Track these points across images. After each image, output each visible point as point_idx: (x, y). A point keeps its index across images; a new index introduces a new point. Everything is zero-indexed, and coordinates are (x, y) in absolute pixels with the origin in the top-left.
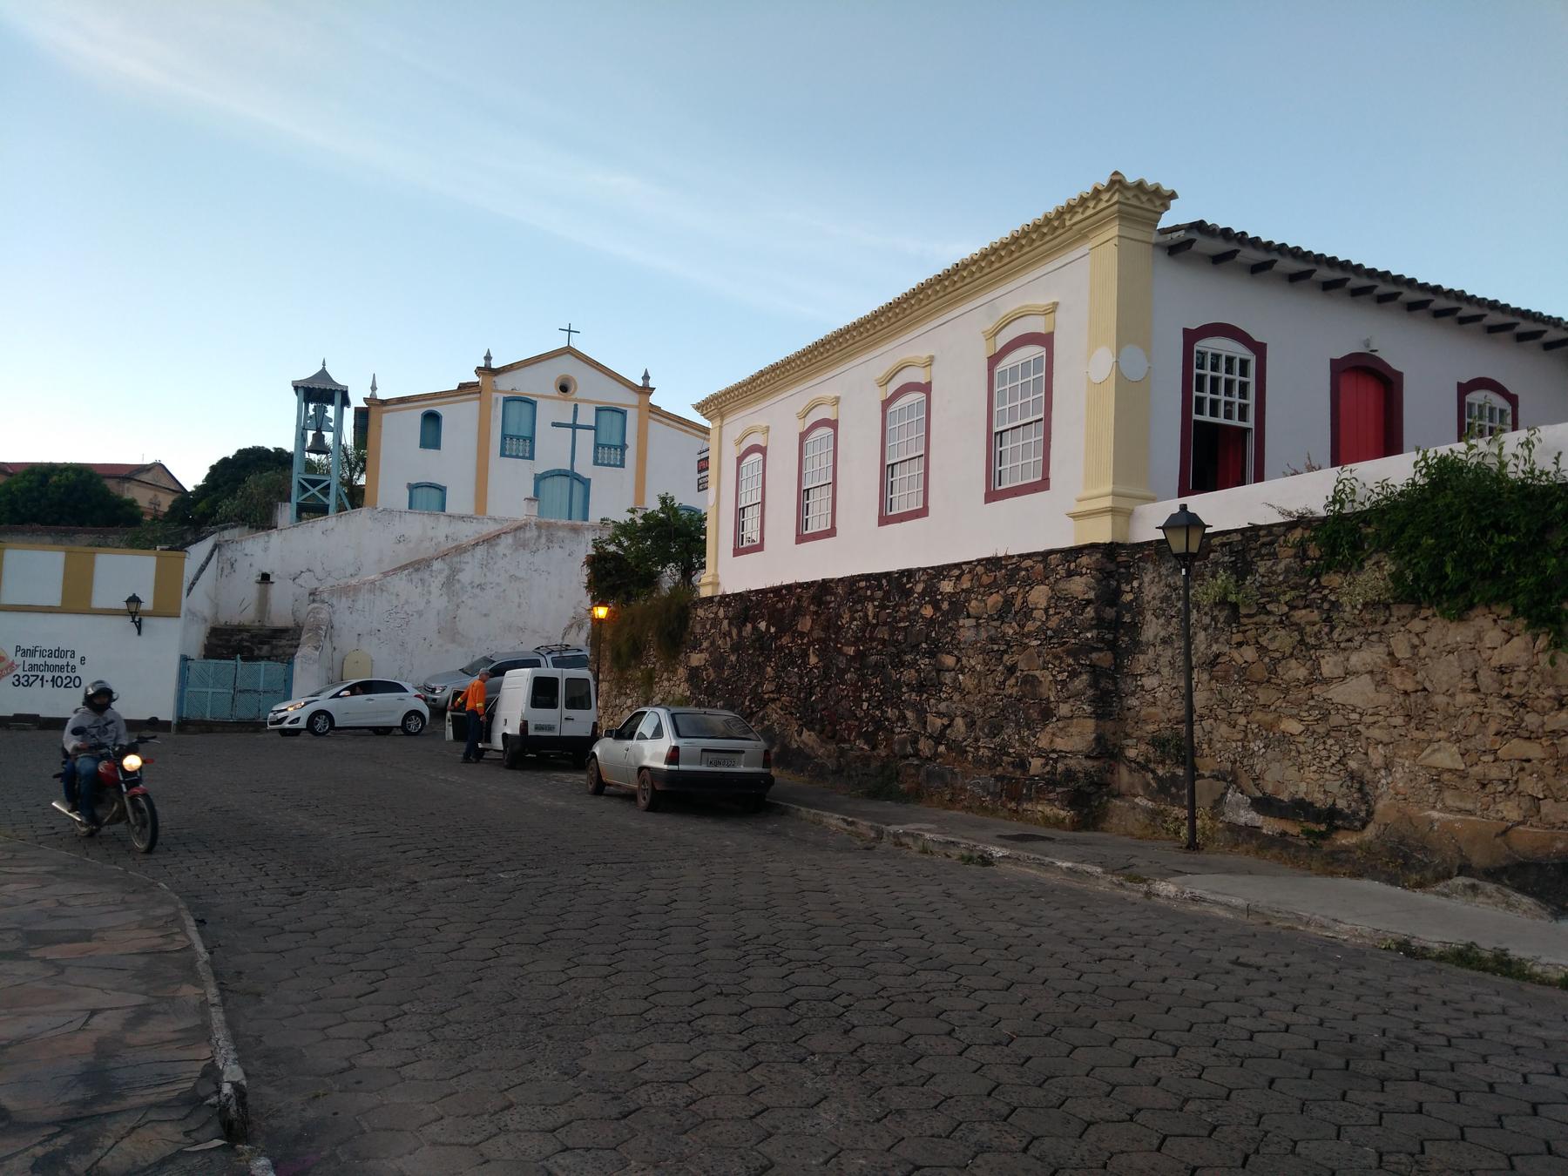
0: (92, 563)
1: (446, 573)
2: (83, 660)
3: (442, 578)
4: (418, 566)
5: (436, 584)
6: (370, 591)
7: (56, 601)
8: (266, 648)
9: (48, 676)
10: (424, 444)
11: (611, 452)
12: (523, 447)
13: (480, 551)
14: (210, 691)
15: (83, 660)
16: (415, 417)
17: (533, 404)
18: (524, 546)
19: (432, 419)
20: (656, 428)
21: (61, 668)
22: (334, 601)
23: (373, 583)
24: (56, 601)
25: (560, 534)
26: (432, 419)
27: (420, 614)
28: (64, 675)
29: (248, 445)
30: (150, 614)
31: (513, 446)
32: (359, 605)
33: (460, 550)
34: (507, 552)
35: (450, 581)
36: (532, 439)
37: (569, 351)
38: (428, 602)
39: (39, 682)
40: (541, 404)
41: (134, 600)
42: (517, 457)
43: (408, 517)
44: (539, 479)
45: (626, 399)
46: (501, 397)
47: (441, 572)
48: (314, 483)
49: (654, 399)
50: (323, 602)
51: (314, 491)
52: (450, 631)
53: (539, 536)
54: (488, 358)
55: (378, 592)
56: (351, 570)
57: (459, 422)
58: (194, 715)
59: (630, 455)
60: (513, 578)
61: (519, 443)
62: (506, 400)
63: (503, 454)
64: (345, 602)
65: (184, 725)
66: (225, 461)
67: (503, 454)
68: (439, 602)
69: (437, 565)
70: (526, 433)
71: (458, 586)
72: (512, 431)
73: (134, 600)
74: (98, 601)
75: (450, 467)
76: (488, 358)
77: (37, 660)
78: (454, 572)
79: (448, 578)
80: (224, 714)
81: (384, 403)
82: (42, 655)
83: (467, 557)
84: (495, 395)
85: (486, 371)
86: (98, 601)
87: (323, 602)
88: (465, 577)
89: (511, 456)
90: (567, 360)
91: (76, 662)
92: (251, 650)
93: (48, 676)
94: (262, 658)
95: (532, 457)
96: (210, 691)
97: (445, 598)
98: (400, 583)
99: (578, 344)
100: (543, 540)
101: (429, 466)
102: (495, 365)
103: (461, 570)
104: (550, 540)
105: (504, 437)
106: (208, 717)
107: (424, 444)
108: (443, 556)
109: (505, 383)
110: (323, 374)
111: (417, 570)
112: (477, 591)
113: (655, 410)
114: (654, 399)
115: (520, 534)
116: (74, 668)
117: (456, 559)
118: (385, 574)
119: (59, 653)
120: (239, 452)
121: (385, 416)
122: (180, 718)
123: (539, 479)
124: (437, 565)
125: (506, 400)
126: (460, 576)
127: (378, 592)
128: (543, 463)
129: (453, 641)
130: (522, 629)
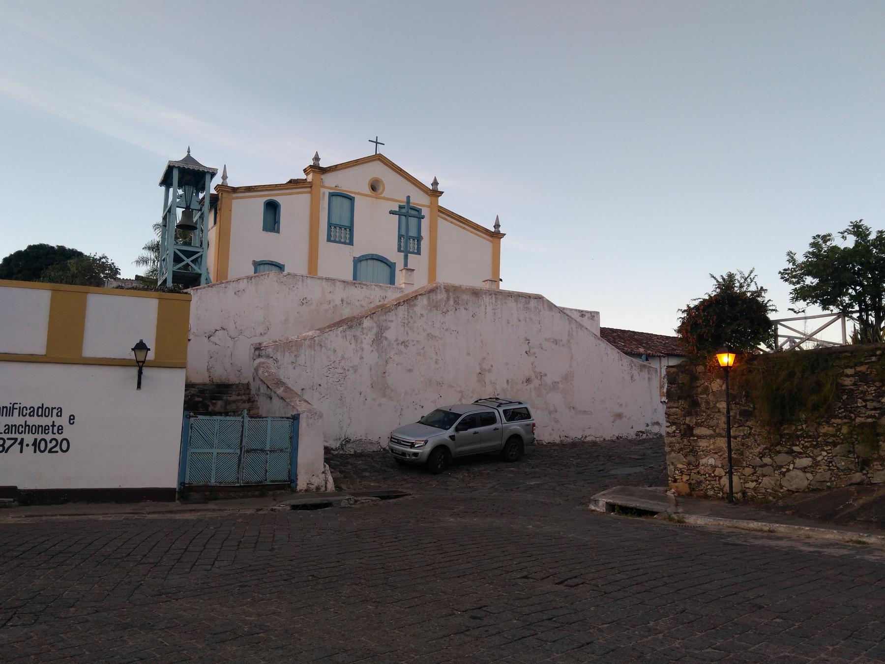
0: (86, 299)
1: (375, 330)
2: (72, 418)
3: (371, 336)
4: (351, 323)
6: (311, 347)
7: (39, 347)
9: (29, 438)
10: (266, 228)
11: (409, 242)
12: (345, 234)
13: (402, 310)
14: (215, 451)
15: (72, 418)
16: (258, 204)
17: (351, 199)
18: (436, 307)
19: (272, 207)
20: (444, 225)
21: (45, 429)
22: (279, 356)
23: (312, 338)
24: (39, 347)
25: (465, 297)
26: (272, 207)
27: (355, 369)
28: (48, 437)
29: (36, 242)
30: (156, 365)
32: (301, 360)
33: (384, 309)
34: (424, 312)
35: (379, 338)
36: (351, 228)
37: (379, 158)
39: (17, 447)
40: (358, 200)
41: (141, 347)
42: (340, 242)
43: (309, 281)
44: (357, 261)
47: (370, 329)
49: (442, 202)
50: (268, 357)
51: (188, 261)
52: (381, 385)
53: (448, 299)
54: (317, 158)
55: (317, 348)
56: (261, 329)
57: (294, 208)
58: (198, 480)
59: (425, 244)
60: (430, 336)
61: (342, 231)
62: (332, 195)
63: (329, 240)
65: (186, 493)
66: (19, 253)
67: (329, 240)
68: (371, 358)
69: (367, 323)
70: (346, 223)
71: (385, 343)
72: (335, 221)
73: (141, 347)
74: (90, 350)
76: (317, 158)
77: (16, 420)
80: (230, 477)
81: (235, 190)
82: (21, 413)
83: (391, 316)
84: (322, 190)
85: (315, 168)
86: (90, 350)
87: (268, 357)
91: (63, 421)
92: (206, 406)
93: (29, 438)
94: (216, 414)
95: (351, 243)
96: (215, 451)
97: (375, 354)
98: (336, 339)
99: (381, 150)
100: (451, 302)
101: (270, 246)
102: (323, 164)
103: (387, 328)
104: (456, 302)
105: (330, 226)
106: (213, 482)
107: (266, 228)
108: (372, 314)
109: (331, 181)
110: (189, 159)
111: (350, 327)
112: (402, 348)
113: (442, 210)
114: (442, 202)
115: (433, 296)
116: (60, 429)
117: (382, 318)
118: (322, 330)
119: (43, 411)
120: (30, 247)
121: (234, 202)
122: (182, 483)
123: (357, 261)
124: (367, 323)
125: (332, 195)
126: (387, 334)
127: (317, 348)
128: (362, 247)
129: (384, 395)
130: (439, 384)
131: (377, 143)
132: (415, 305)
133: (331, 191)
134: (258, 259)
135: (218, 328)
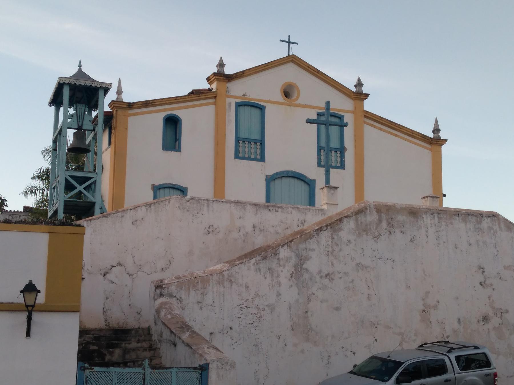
1: (293, 261)
3: (289, 268)
4: (265, 253)
5: (285, 273)
6: (219, 283)
8: (118, 352)
11: (331, 155)
12: (255, 149)
13: (325, 236)
16: (156, 121)
17: (262, 109)
19: (172, 123)
20: (371, 133)
22: (183, 295)
23: (221, 273)
25: (400, 218)
26: (172, 123)
27: (272, 308)
31: (245, 148)
32: (209, 299)
33: (304, 236)
34: (352, 237)
35: (298, 271)
36: (262, 142)
37: (292, 60)
38: (279, 294)
40: (270, 111)
41: (30, 289)
42: (249, 159)
43: (215, 205)
44: (270, 180)
45: (340, 104)
46: (233, 102)
47: (288, 259)
48: (82, 180)
49: (368, 106)
50: (171, 296)
53: (380, 221)
54: (221, 65)
56: (161, 264)
57: (197, 123)
59: (349, 157)
60: (360, 266)
61: (252, 146)
62: (239, 105)
63: (237, 157)
64: (191, 298)
67: (237, 157)
68: (290, 294)
69: (284, 253)
70: (257, 137)
71: (306, 276)
72: (243, 134)
75: (193, 164)
76: (221, 65)
78: (301, 261)
79: (296, 267)
81: (130, 106)
83: (312, 244)
84: (228, 100)
85: (220, 76)
87: (171, 296)
88: (312, 265)
89: (244, 158)
90: (291, 69)
92: (102, 356)
95: (262, 159)
98: (248, 273)
100: (384, 224)
101: (170, 167)
102: (228, 70)
103: (308, 258)
104: (390, 224)
105: (238, 140)
108: (289, 242)
109: (237, 89)
111: (265, 258)
112: (326, 281)
114: (368, 106)
115: (361, 218)
117: (302, 246)
123: (270, 180)
124: (284, 253)
125: (239, 105)
126: (308, 265)
127: (227, 284)
128: (275, 163)
129: (308, 340)
130: (373, 324)
131: (289, 42)
132: (340, 229)
133: (239, 101)
134: (157, 183)
135: (115, 264)
